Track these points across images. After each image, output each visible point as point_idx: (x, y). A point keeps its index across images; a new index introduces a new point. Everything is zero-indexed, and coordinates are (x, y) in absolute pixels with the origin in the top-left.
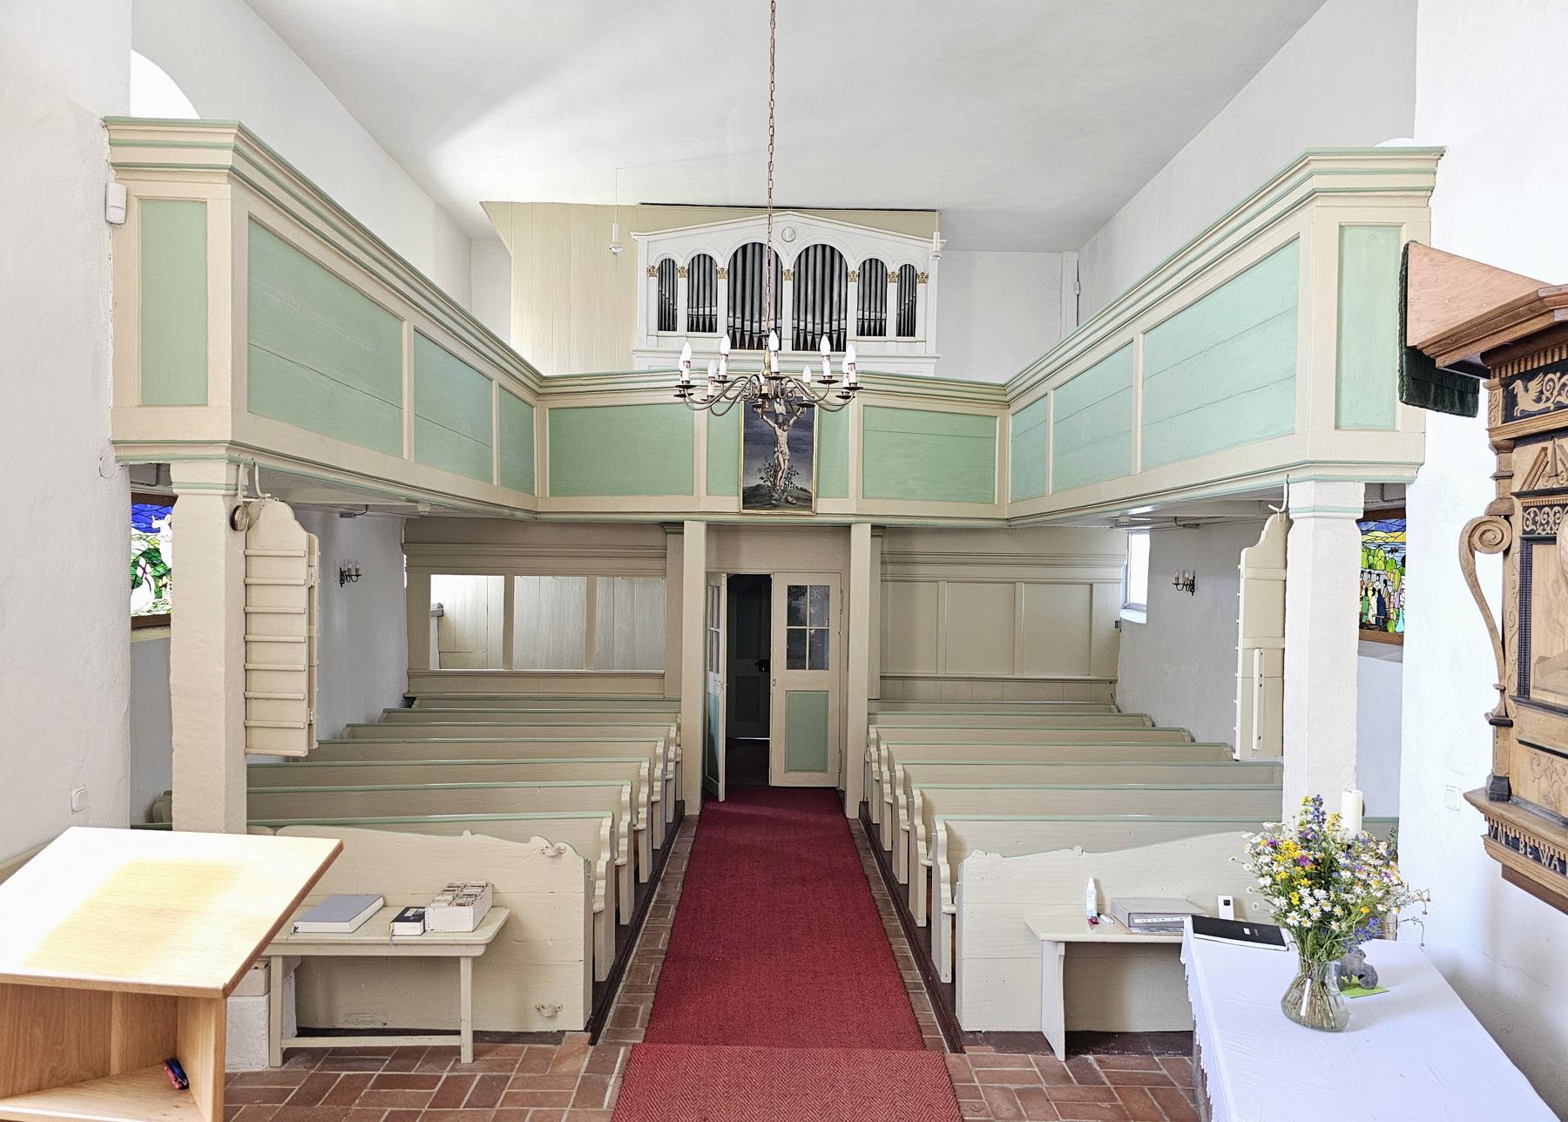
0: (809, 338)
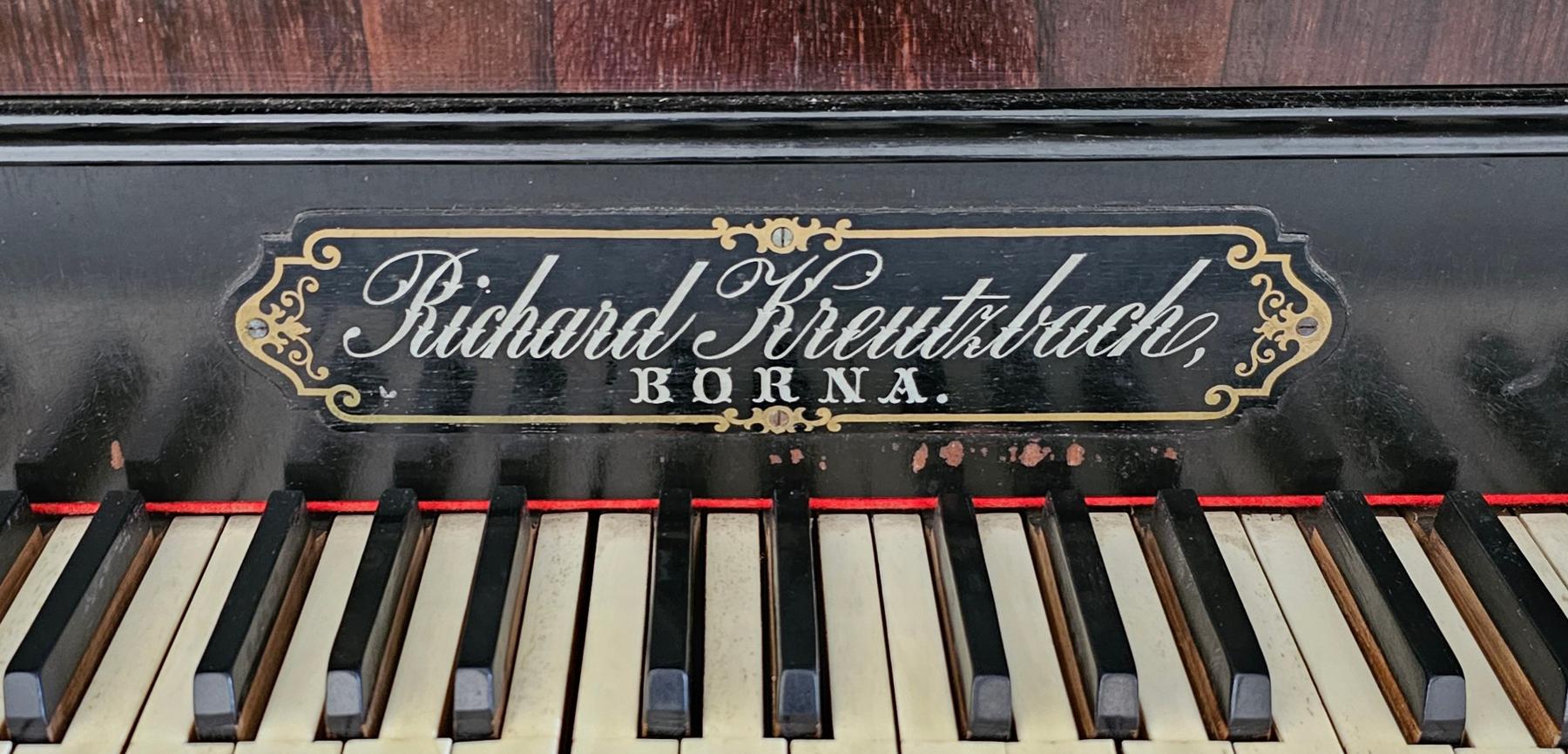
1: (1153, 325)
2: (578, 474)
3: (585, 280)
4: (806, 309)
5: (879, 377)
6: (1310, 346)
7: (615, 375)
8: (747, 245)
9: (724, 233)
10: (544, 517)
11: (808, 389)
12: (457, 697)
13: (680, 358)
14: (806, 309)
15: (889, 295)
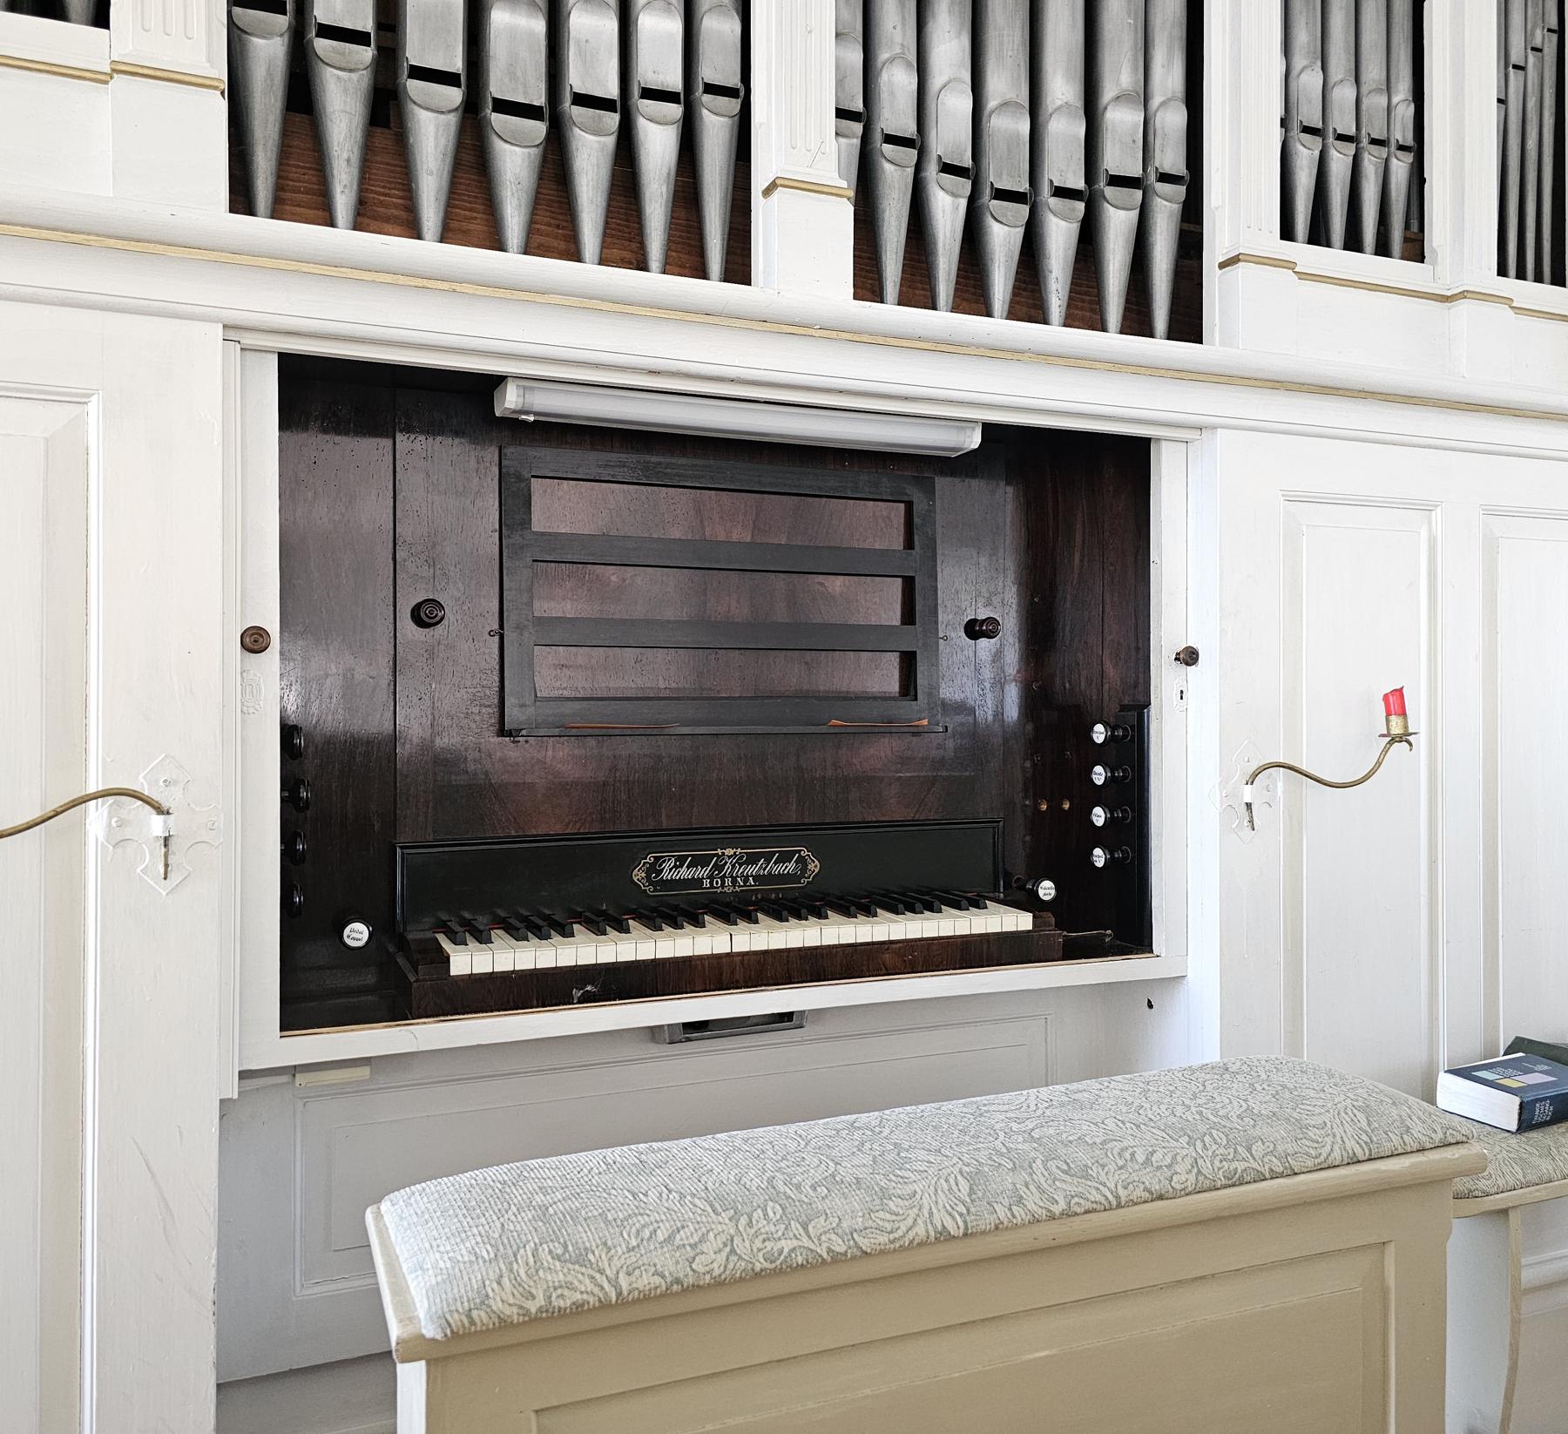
0: (947, 210)
1: (791, 867)
5: (746, 879)
7: (700, 881)
9: (719, 852)
13: (711, 877)
15: (747, 863)
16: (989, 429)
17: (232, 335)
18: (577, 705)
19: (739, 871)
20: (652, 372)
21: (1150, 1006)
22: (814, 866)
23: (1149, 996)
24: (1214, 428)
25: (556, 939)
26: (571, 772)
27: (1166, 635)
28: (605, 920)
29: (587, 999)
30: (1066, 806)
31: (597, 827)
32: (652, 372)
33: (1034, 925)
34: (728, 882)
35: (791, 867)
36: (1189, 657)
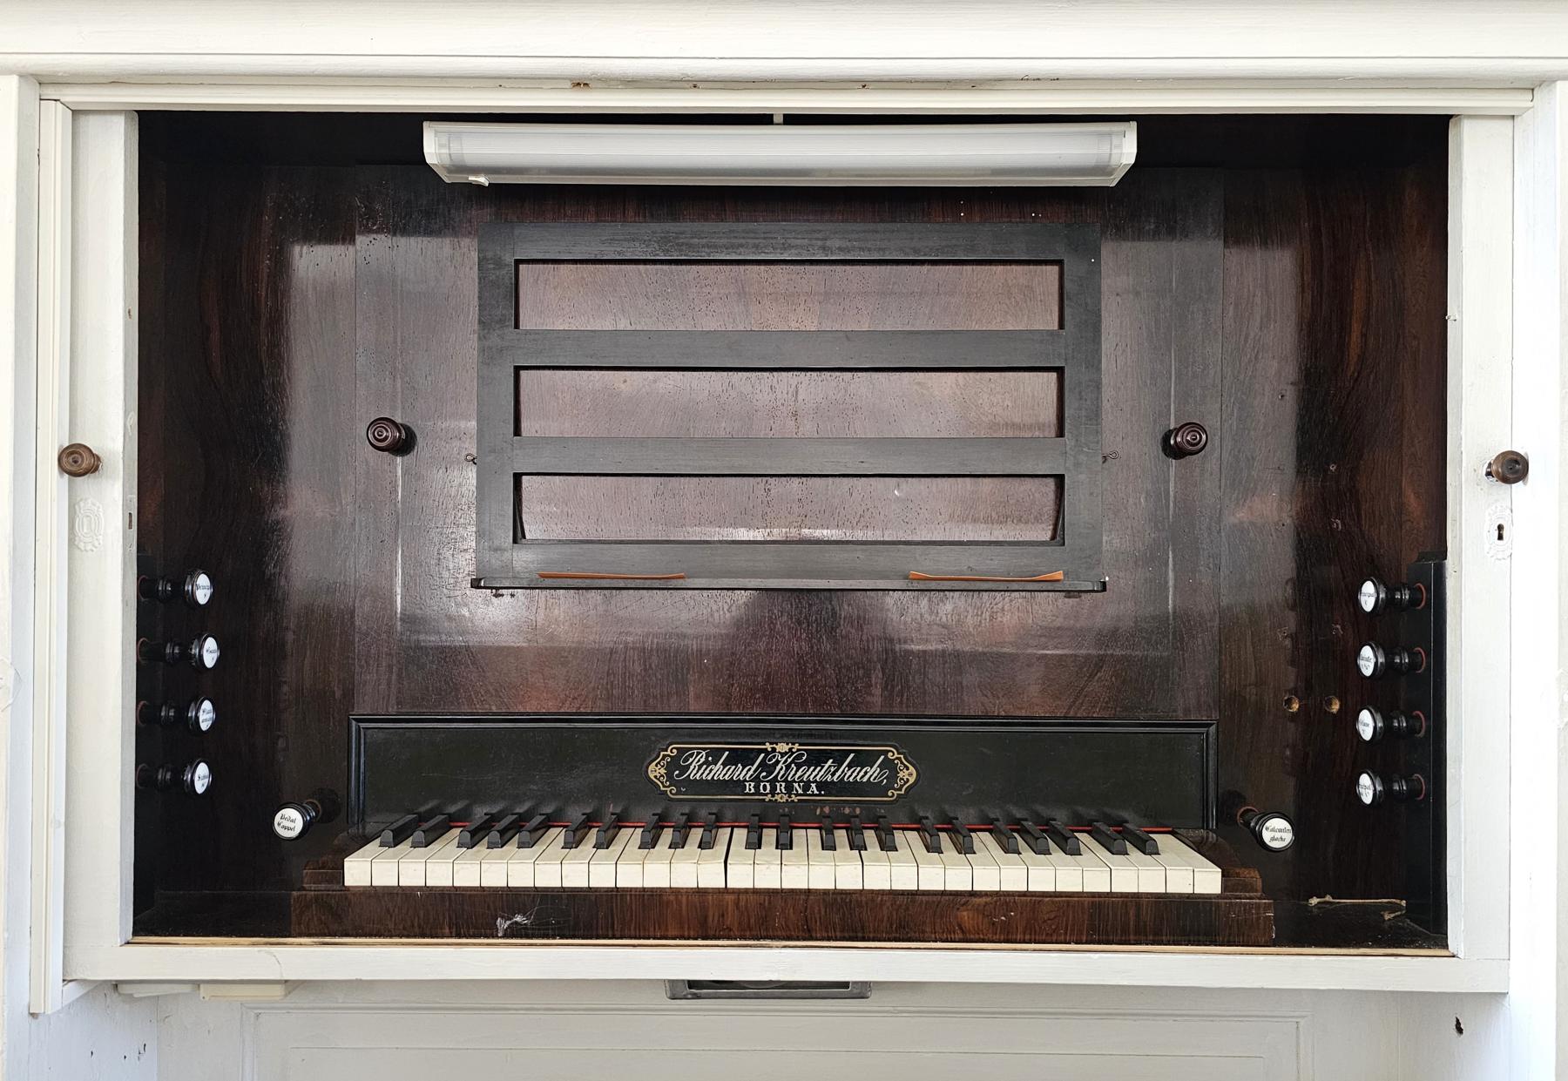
1: (872, 773)
2: (729, 814)
3: (737, 758)
4: (788, 767)
5: (807, 786)
6: (912, 780)
7: (740, 784)
8: (774, 750)
9: (768, 747)
10: (1559, 83)
11: (789, 787)
12: (1052, 496)
13: (757, 780)
14: (788, 767)
15: (808, 763)
16: (1152, 128)
17: (50, 92)
18: (566, 549)
19: (796, 774)
20: (580, 84)
21: (1460, 1030)
22: (909, 775)
23: (1460, 1016)
24: (1532, 85)
25: (1057, 855)
26: (566, 635)
27: (1472, 435)
28: (596, 825)
29: (515, 932)
30: (1336, 707)
31: (601, 707)
32: (580, 84)
33: (1225, 887)
34: (780, 787)
35: (872, 773)
36: (1512, 468)
